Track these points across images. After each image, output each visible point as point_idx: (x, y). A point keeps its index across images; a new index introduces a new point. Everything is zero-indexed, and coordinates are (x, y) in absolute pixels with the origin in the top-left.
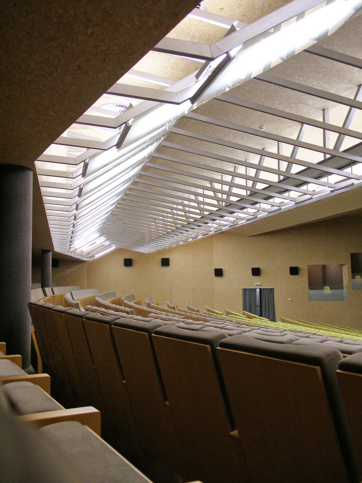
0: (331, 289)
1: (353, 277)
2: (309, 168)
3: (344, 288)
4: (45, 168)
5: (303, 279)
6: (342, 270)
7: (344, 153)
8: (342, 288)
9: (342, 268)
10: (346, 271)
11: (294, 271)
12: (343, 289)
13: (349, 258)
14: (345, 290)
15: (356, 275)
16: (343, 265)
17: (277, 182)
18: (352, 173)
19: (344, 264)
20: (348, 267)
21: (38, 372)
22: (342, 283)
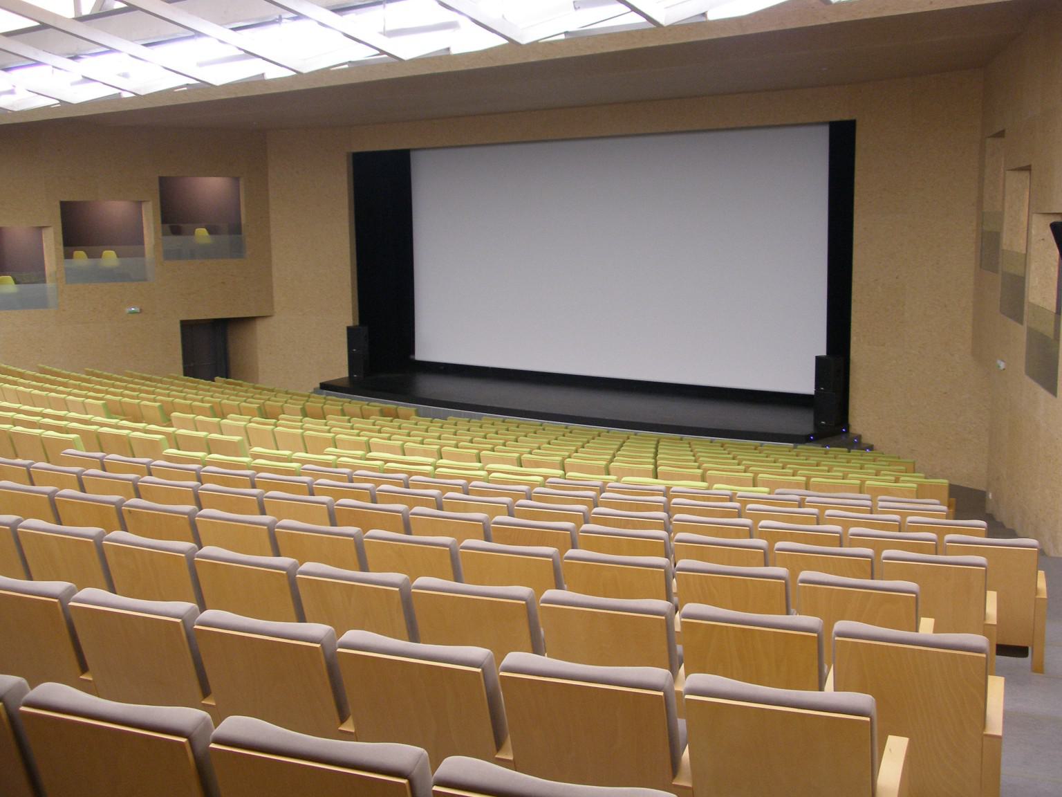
0: (16, 282)
1: (68, 256)
2: (43, 26)
3: (48, 281)
4: (689, 760)
6: (42, 240)
7: (5, 37)
8: (42, 278)
9: (141, 208)
10: (51, 242)
12: (44, 282)
13: (156, 186)
14: (50, 284)
15: (75, 250)
16: (44, 227)
17: (74, 19)
18: (842, 143)
19: (142, 200)
20: (55, 233)
21: (67, 248)
22: (43, 269)
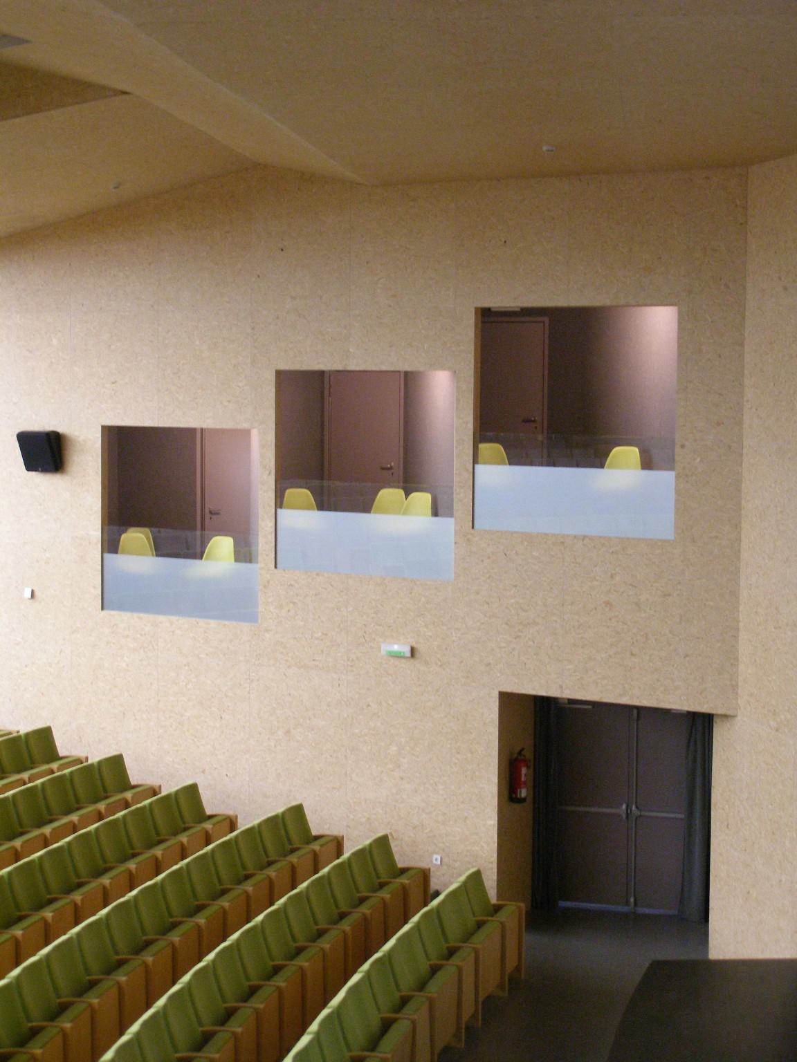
5: (82, 490)
11: (44, 452)
